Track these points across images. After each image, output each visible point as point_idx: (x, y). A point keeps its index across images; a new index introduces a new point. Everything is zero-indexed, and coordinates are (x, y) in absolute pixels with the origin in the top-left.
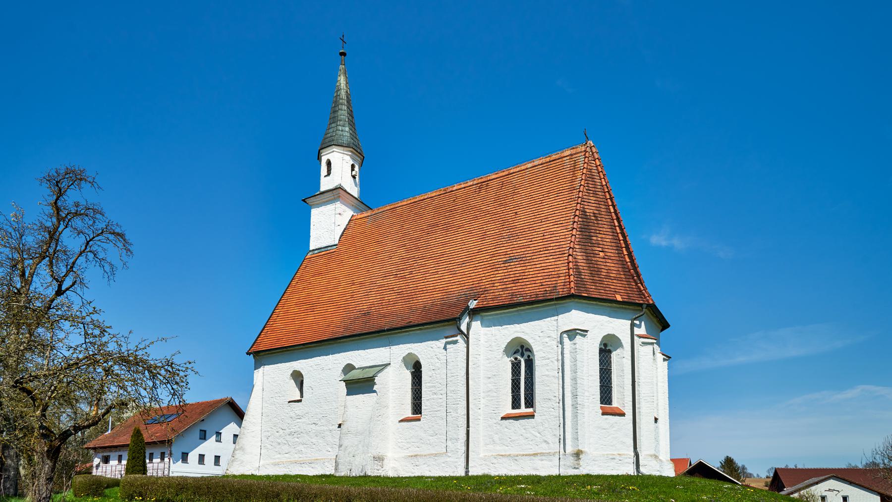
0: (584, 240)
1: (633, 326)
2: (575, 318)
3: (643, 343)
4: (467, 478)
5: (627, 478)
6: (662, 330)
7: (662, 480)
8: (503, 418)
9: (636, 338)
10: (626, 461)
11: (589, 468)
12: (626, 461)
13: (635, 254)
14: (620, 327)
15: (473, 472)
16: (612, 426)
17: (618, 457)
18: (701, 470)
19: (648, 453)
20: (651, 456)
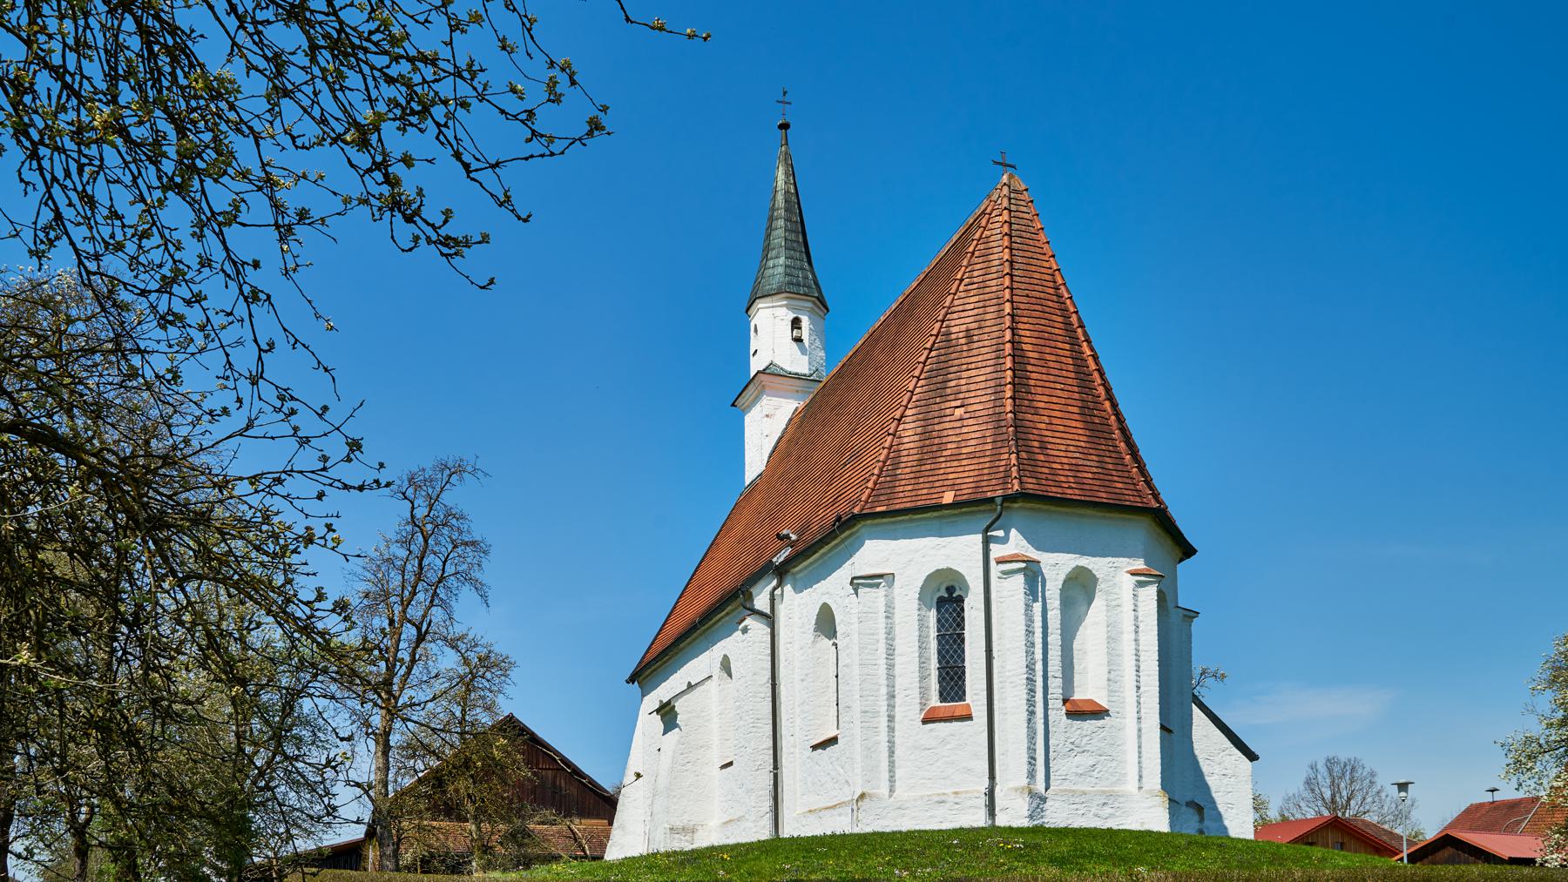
0: (923, 409)
1: (987, 542)
2: (874, 553)
3: (1004, 573)
4: (775, 847)
5: (968, 838)
6: (1181, 560)
7: (1145, 839)
8: (815, 748)
9: (993, 564)
10: (969, 803)
11: (879, 817)
12: (969, 803)
13: (1129, 423)
14: (959, 552)
15: (787, 831)
16: (944, 741)
17: (952, 798)
18: (1340, 831)
19: (1011, 785)
20: (1016, 790)
